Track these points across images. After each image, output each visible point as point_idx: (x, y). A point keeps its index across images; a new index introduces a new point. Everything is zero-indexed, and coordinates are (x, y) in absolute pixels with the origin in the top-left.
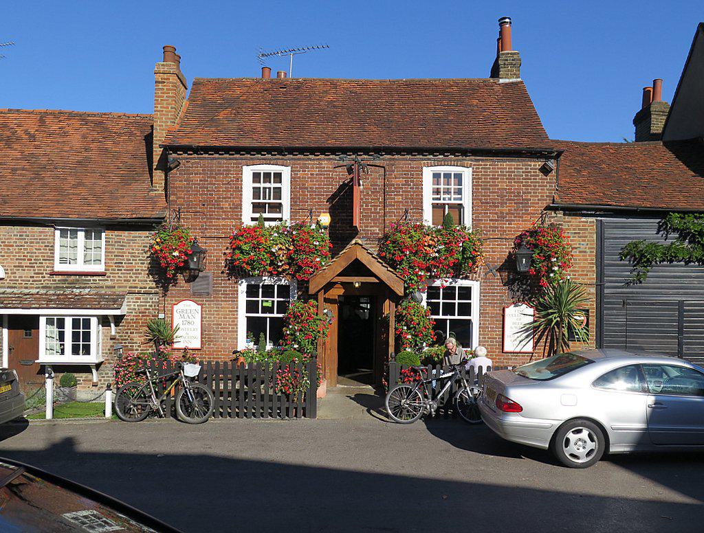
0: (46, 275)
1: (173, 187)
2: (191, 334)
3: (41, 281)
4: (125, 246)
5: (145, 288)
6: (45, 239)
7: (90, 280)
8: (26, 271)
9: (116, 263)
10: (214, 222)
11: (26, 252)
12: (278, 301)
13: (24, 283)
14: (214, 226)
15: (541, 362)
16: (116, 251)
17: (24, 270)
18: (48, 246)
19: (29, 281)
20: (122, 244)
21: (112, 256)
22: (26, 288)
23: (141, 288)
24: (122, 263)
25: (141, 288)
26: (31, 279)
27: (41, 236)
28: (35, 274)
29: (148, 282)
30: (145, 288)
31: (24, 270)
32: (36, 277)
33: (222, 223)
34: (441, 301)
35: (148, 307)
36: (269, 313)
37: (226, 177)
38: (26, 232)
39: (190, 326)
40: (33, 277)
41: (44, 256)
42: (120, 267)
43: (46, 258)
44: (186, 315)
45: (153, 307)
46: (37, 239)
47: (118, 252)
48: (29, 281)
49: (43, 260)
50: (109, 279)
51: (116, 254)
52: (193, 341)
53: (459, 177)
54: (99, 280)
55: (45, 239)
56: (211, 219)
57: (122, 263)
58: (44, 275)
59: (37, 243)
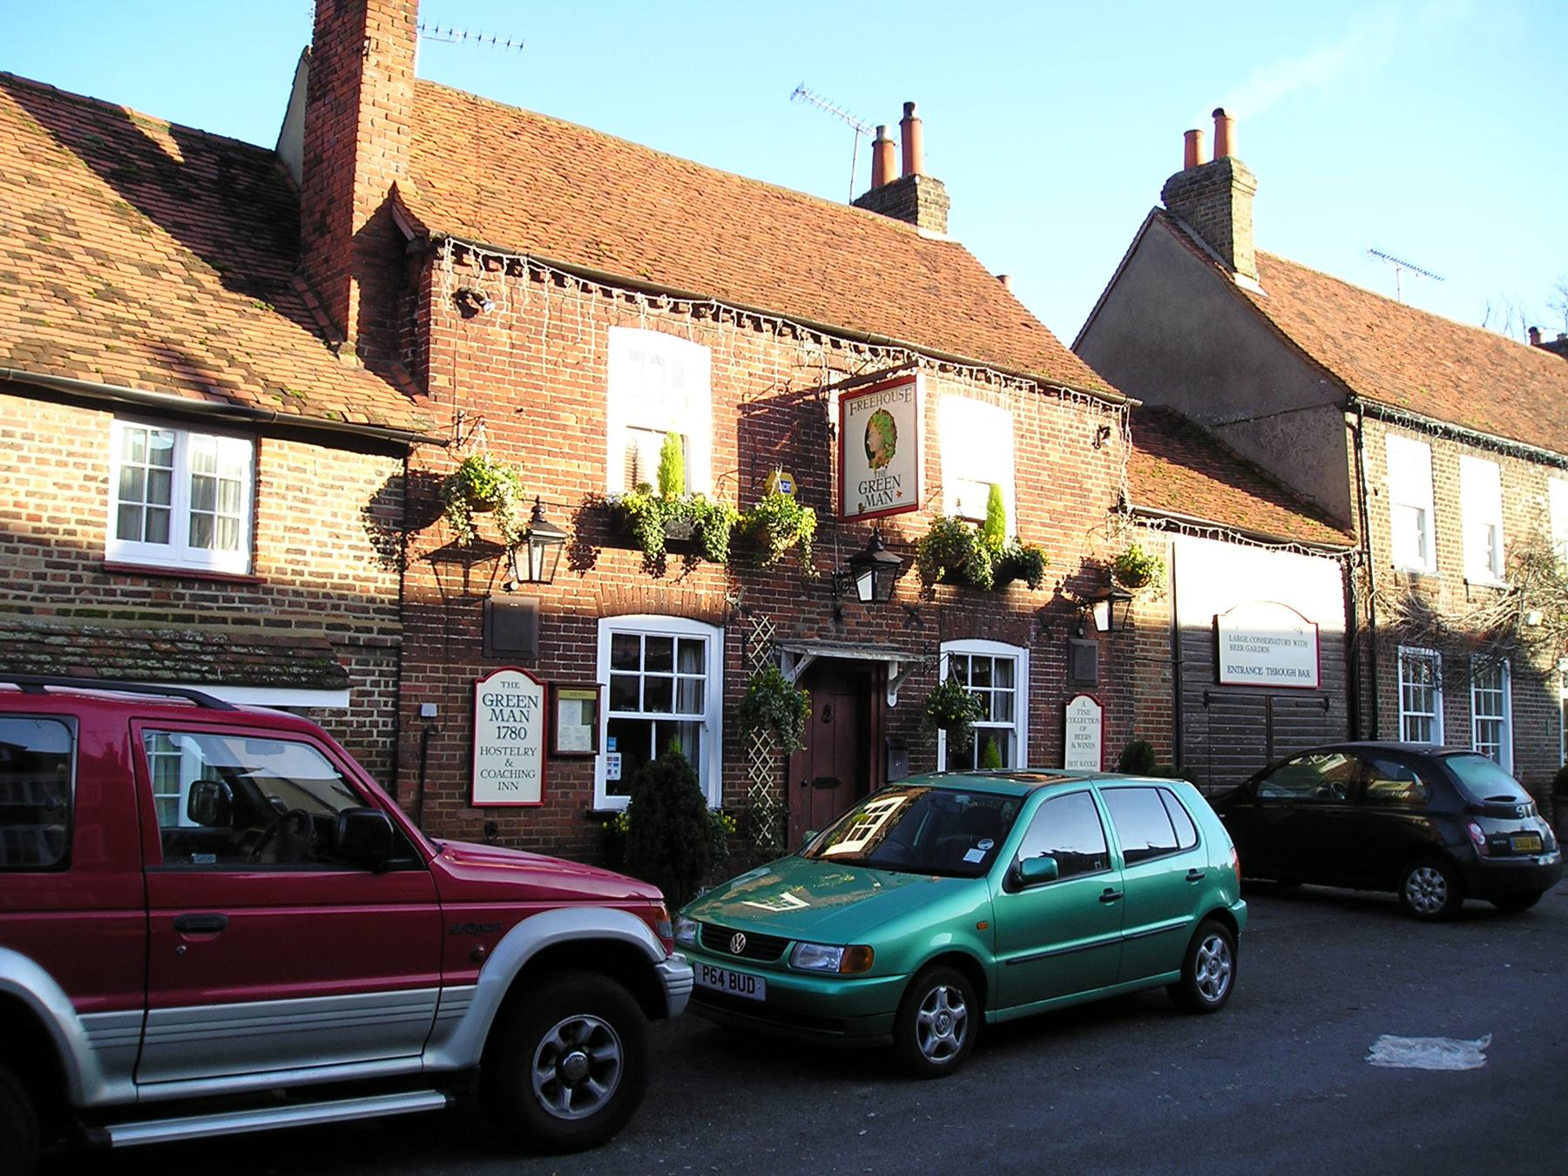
0: (85, 574)
1: (444, 353)
2: (520, 763)
3: (67, 590)
4: (313, 503)
5: (369, 630)
6: (84, 455)
7: (214, 599)
8: (21, 555)
9: (288, 551)
10: (545, 462)
11: (22, 489)
12: (646, 670)
13: (12, 593)
14: (542, 471)
15: (454, 803)
16: (290, 514)
17: (15, 551)
18: (94, 479)
19: (29, 588)
20: (304, 495)
21: (277, 528)
22: (27, 611)
23: (358, 630)
24: (303, 553)
25: (358, 630)
26: (37, 583)
27: (72, 442)
28: (48, 565)
29: (372, 614)
30: (369, 630)
31: (15, 551)
32: (54, 577)
33: (561, 465)
34: (642, 673)
35: (368, 688)
36: (659, 710)
37: (572, 349)
38: (25, 425)
39: (518, 743)
40: (43, 577)
41: (81, 511)
42: (298, 562)
43: (86, 517)
44: (507, 712)
45: (382, 688)
46: (60, 452)
47: (296, 519)
48: (29, 588)
49: (79, 522)
50: (269, 597)
51: (289, 523)
52: (523, 782)
53: (1006, 665)
54: (242, 600)
55: (84, 455)
56: (536, 451)
57: (303, 553)
58: (79, 572)
59: (59, 464)
